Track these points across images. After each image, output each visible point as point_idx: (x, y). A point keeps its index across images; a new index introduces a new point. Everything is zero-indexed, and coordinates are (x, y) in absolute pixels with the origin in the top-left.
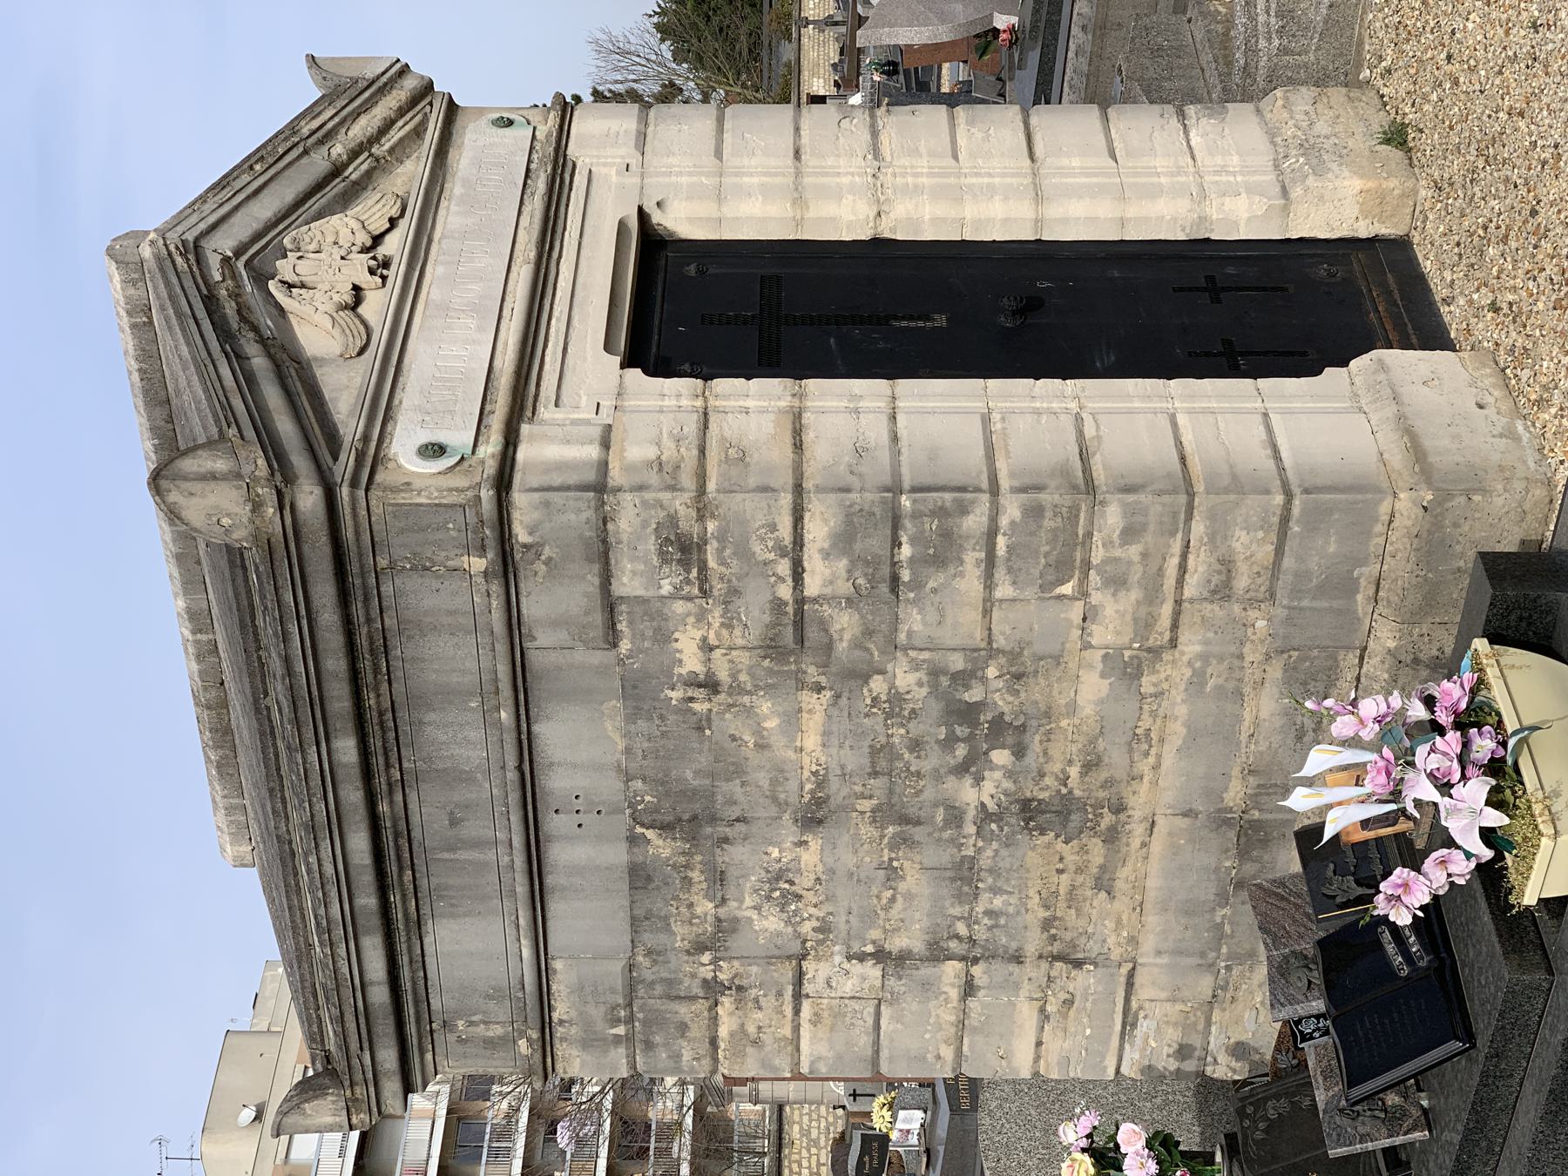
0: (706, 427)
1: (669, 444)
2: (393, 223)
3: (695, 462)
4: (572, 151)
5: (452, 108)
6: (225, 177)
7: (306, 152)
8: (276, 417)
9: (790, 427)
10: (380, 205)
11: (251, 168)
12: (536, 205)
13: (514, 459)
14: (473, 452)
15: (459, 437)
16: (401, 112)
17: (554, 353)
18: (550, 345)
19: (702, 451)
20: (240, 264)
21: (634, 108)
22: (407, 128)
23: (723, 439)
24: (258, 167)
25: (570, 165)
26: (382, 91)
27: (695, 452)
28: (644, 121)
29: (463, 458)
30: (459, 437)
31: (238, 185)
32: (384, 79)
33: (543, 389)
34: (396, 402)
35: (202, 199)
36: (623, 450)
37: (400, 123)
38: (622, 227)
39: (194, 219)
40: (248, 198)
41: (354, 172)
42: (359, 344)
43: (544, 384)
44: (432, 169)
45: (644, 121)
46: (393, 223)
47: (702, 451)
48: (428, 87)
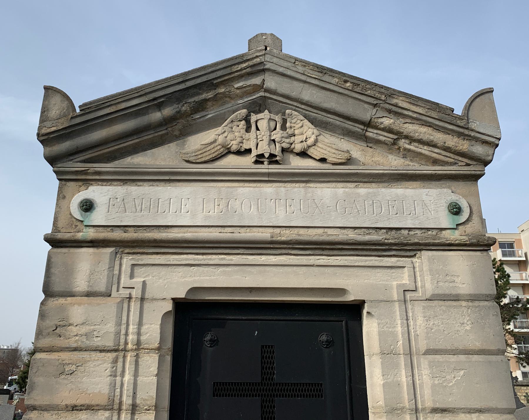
0: (101, 351)
1: (84, 330)
2: (323, 160)
3: (63, 346)
4: (426, 255)
5: (476, 178)
6: (332, 71)
7: (375, 105)
8: (108, 129)
9: (93, 403)
10: (334, 151)
11: (346, 81)
12: (352, 236)
13: (82, 247)
14: (86, 226)
15: (98, 217)
16: (447, 149)
17: (186, 259)
18: (295, 257)
19: (75, 349)
20: (262, 94)
21: (494, 291)
22: (434, 155)
23: (86, 362)
24: (348, 84)
25: (412, 253)
26: (460, 135)
27: (74, 345)
28: (486, 298)
29: (82, 221)
30: (98, 217)
31: (326, 78)
32: (473, 134)
33: (149, 256)
34: (139, 183)
35: (306, 64)
36: (80, 304)
37: (436, 150)
38: (342, 291)
39: (285, 64)
40: (317, 86)
41: (371, 133)
42: (191, 159)
43: (154, 256)
44: (378, 174)
45: (486, 298)
46: (323, 160)
47: (75, 349)
48: (486, 163)
